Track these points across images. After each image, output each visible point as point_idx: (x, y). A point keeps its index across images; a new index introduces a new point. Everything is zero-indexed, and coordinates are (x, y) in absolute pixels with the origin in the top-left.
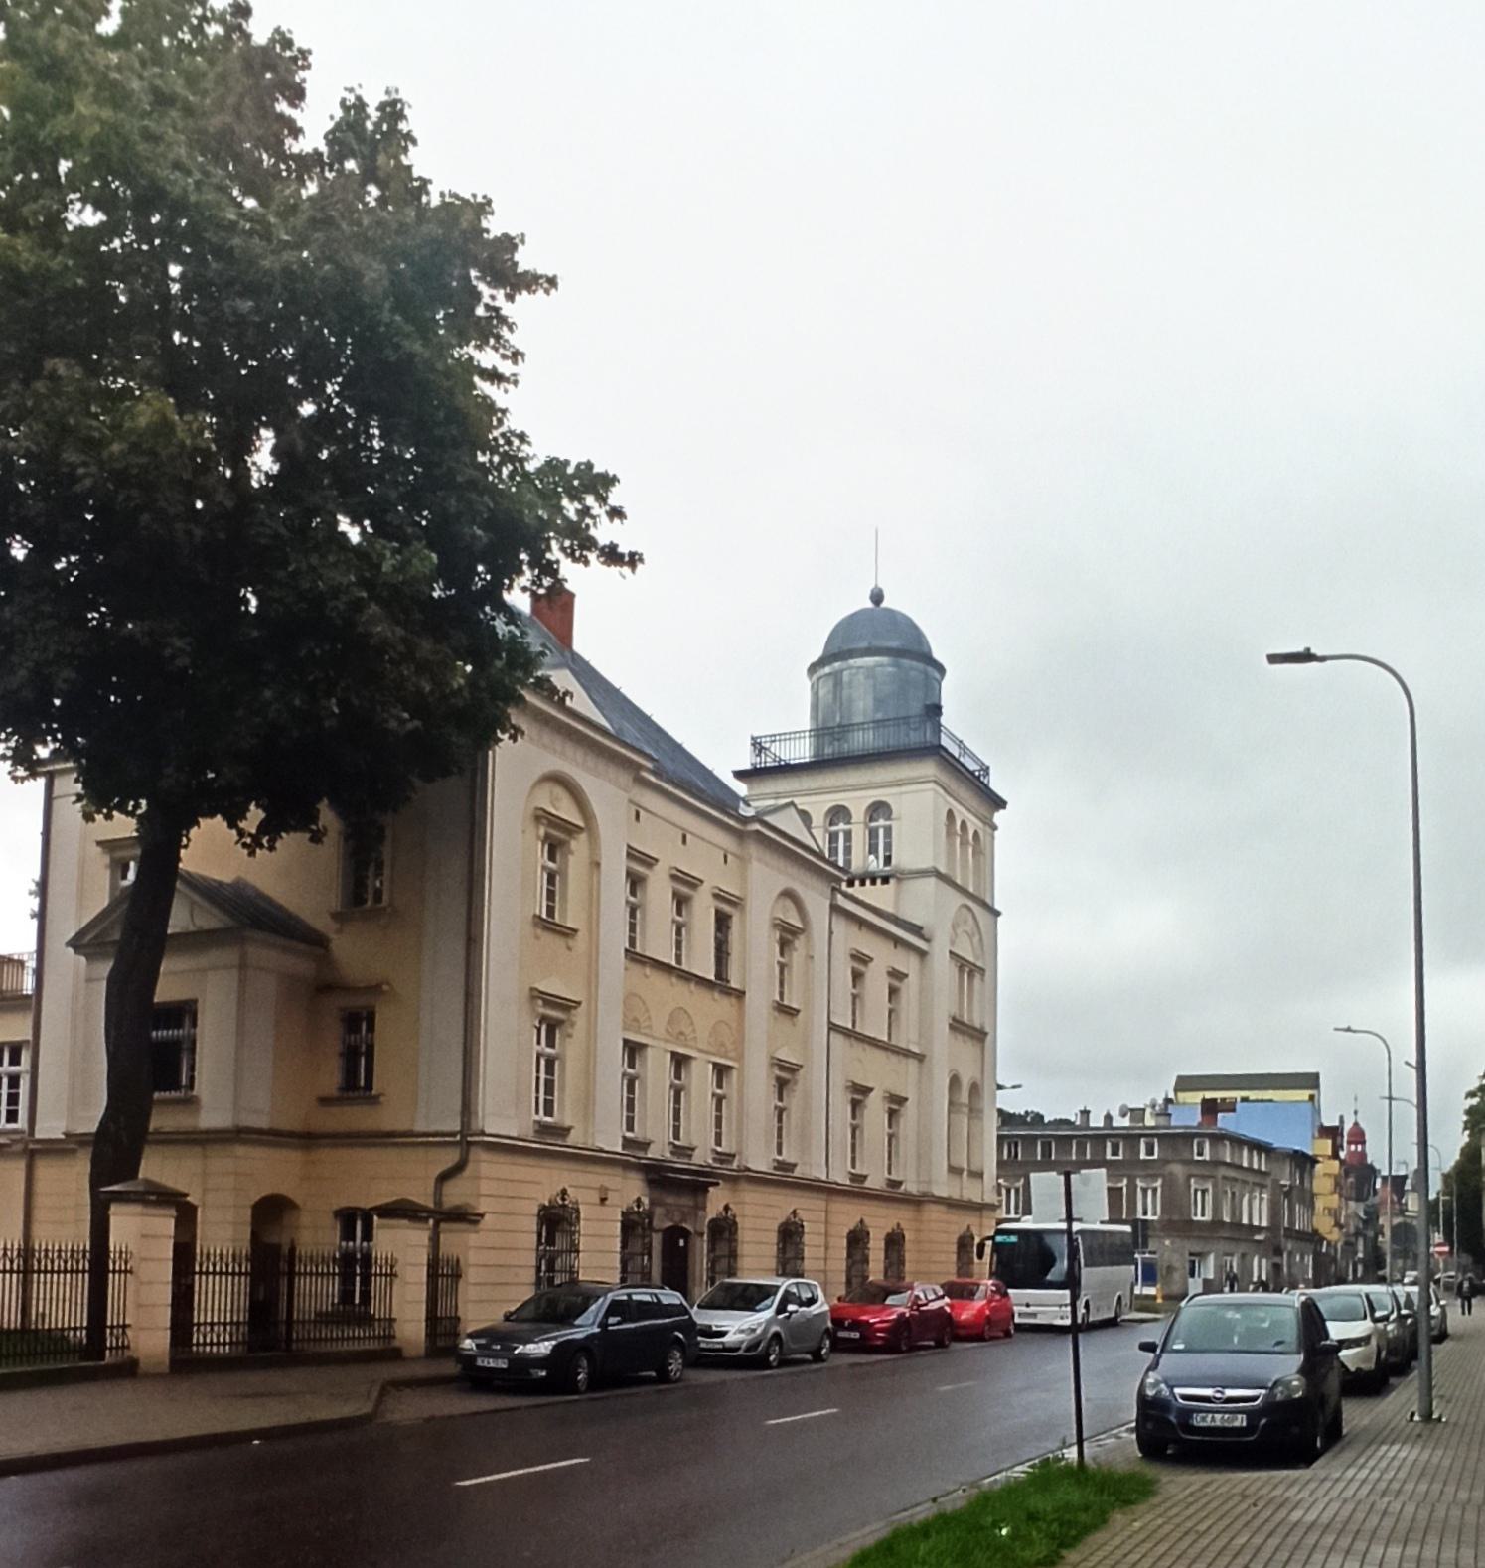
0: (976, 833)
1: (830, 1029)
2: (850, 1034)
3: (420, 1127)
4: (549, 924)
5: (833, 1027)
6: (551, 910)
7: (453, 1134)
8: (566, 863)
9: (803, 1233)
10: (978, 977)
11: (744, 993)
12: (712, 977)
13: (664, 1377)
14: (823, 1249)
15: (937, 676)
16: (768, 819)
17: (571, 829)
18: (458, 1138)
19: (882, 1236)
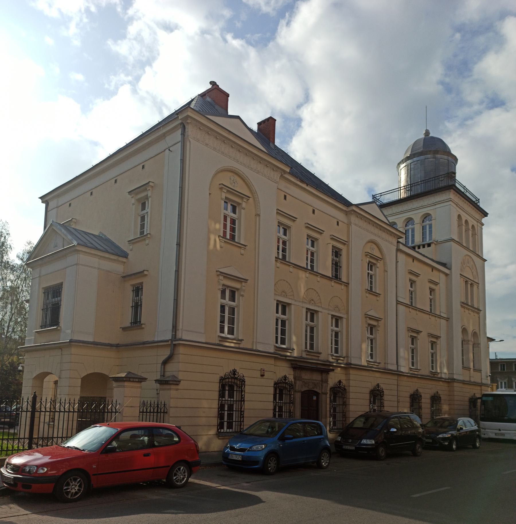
0: (473, 226)
1: (397, 304)
2: (411, 306)
3: (156, 340)
4: (370, 291)
5: (398, 303)
6: (371, 287)
7: (167, 341)
8: (376, 271)
9: (441, 400)
10: (475, 287)
11: (348, 284)
12: (331, 276)
13: (475, 447)
14: (396, 402)
15: (454, 161)
16: (360, 207)
17: (377, 259)
18: (170, 343)
19: (428, 396)
